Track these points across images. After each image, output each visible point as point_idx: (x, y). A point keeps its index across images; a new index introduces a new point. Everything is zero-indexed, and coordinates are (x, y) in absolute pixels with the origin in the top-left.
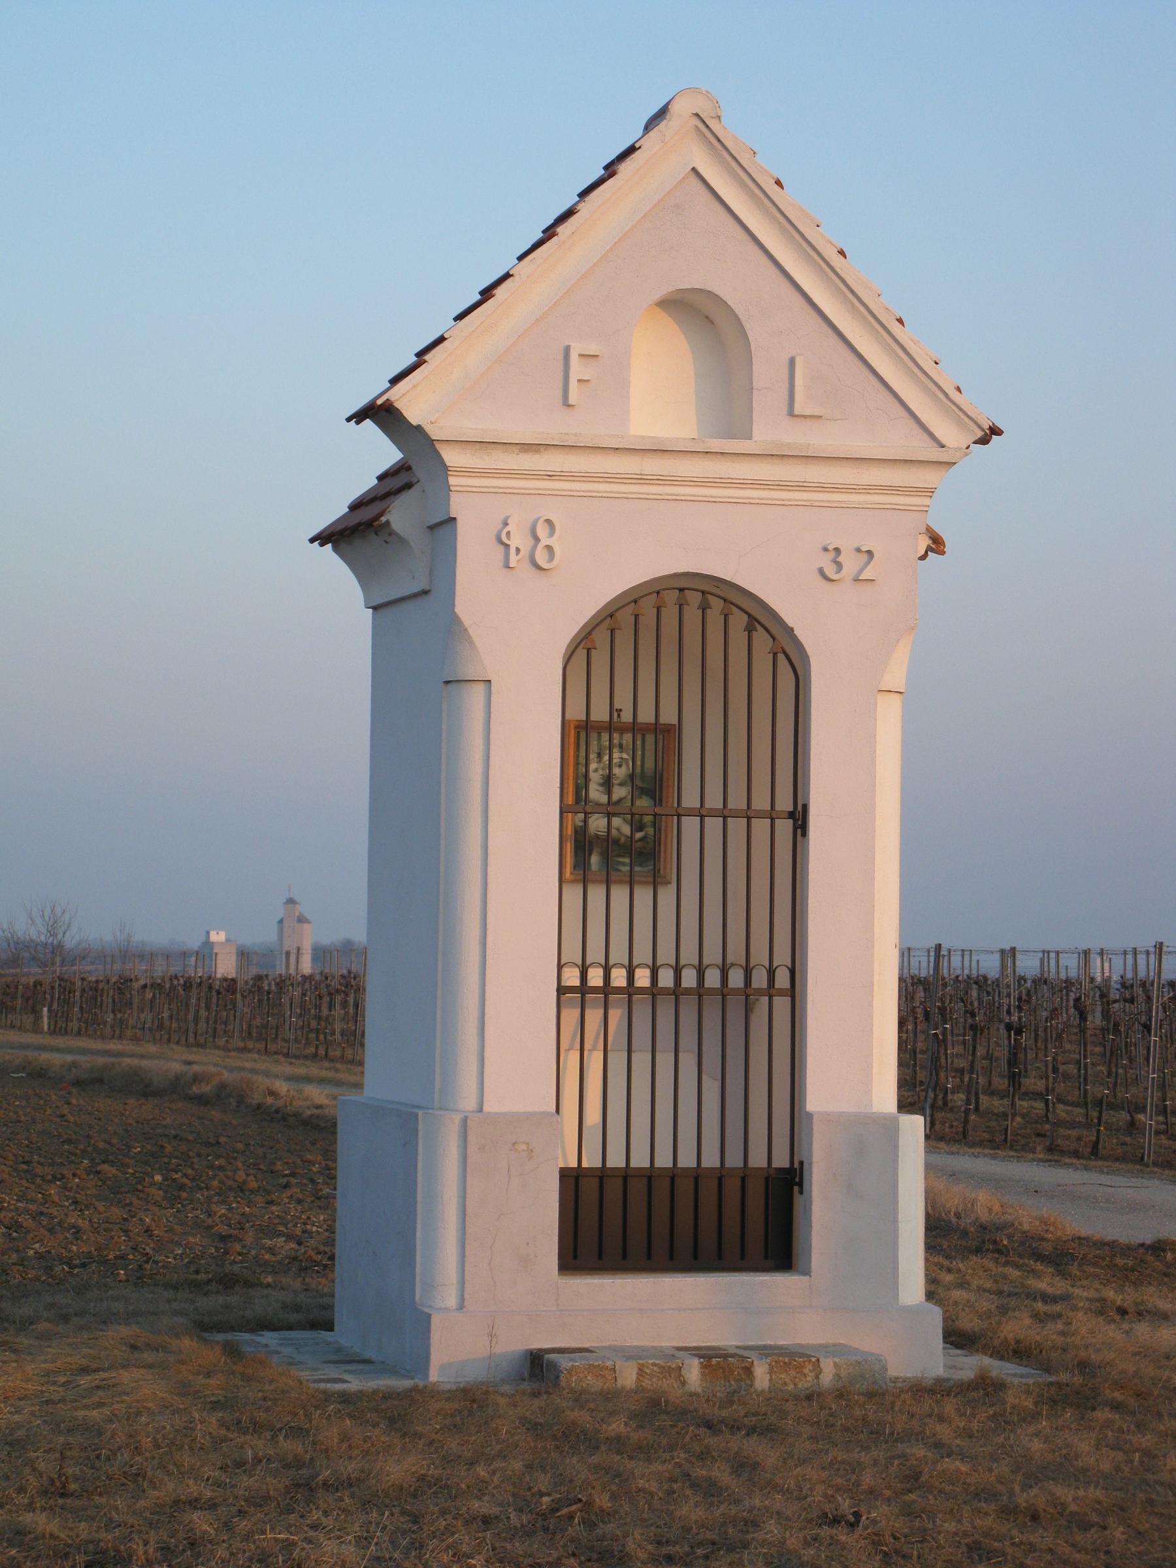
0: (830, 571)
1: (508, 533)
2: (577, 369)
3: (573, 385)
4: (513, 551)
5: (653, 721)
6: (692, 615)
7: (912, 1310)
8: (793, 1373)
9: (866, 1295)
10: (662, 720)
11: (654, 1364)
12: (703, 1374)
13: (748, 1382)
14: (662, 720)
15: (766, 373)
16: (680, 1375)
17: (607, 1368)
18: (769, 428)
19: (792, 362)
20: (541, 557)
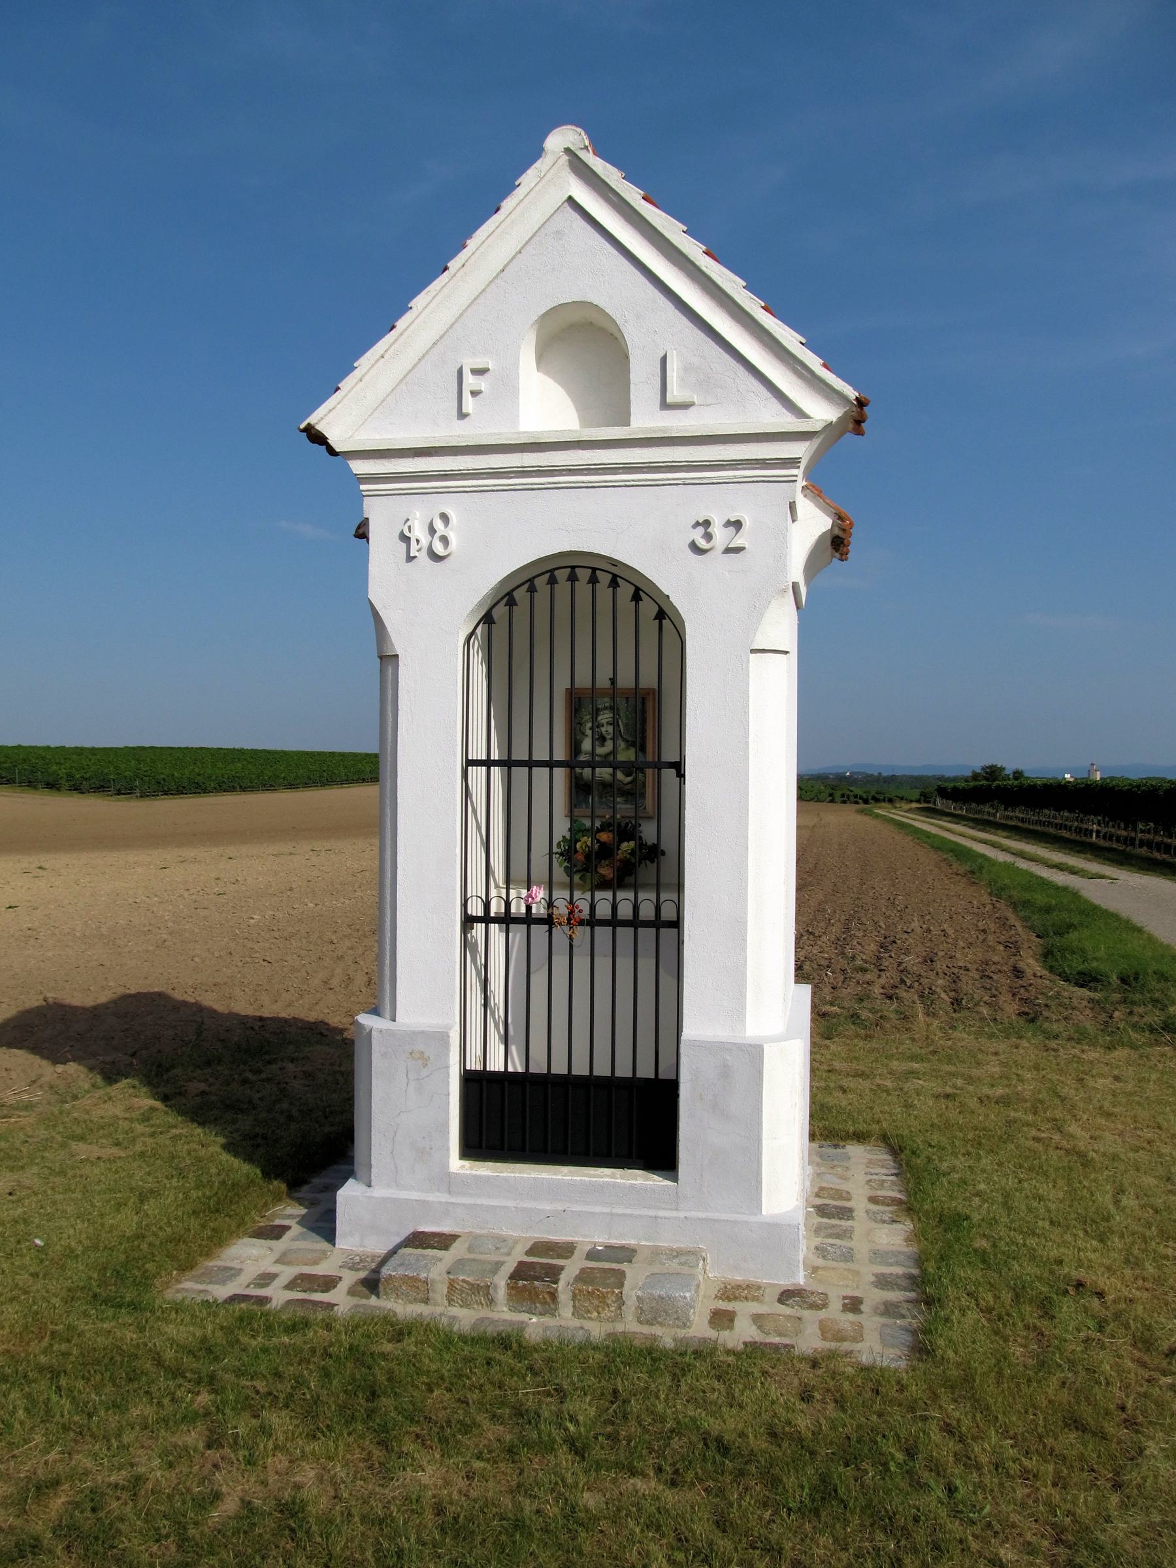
0: (702, 543)
1: (409, 528)
2: (470, 381)
3: (466, 395)
4: (413, 542)
5: (589, 685)
6: (583, 587)
7: (776, 1229)
8: (596, 1302)
9: (765, 1202)
10: (642, 685)
11: (464, 1281)
12: (509, 1295)
13: (553, 1306)
14: (642, 685)
15: (642, 373)
16: (488, 1293)
17: (420, 1281)
18: (645, 417)
19: (664, 360)
20: (439, 548)
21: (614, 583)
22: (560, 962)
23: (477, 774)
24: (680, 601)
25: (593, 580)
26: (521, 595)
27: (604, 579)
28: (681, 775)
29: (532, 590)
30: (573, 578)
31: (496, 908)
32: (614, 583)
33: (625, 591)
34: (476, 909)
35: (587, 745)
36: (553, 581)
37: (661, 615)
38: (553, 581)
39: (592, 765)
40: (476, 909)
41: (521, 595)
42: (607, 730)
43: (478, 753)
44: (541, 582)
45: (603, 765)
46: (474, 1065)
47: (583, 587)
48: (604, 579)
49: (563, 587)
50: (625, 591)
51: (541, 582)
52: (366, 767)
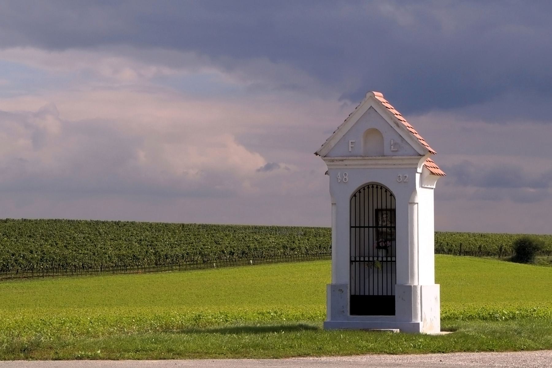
6: (375, 189)
21: (381, 188)
22: (376, 275)
23: (353, 229)
24: (394, 193)
25: (377, 187)
26: (362, 191)
27: (379, 187)
28: (395, 229)
29: (364, 189)
30: (373, 187)
31: (358, 259)
32: (381, 188)
33: (384, 190)
34: (353, 259)
35: (380, 223)
36: (368, 188)
37: (391, 195)
38: (368, 188)
39: (382, 227)
40: (353, 259)
41: (362, 191)
42: (385, 219)
43: (353, 225)
44: (366, 188)
45: (384, 227)
46: (353, 293)
47: (375, 189)
48: (379, 187)
49: (371, 189)
50: (384, 190)
51: (366, 188)
52: (438, 250)
